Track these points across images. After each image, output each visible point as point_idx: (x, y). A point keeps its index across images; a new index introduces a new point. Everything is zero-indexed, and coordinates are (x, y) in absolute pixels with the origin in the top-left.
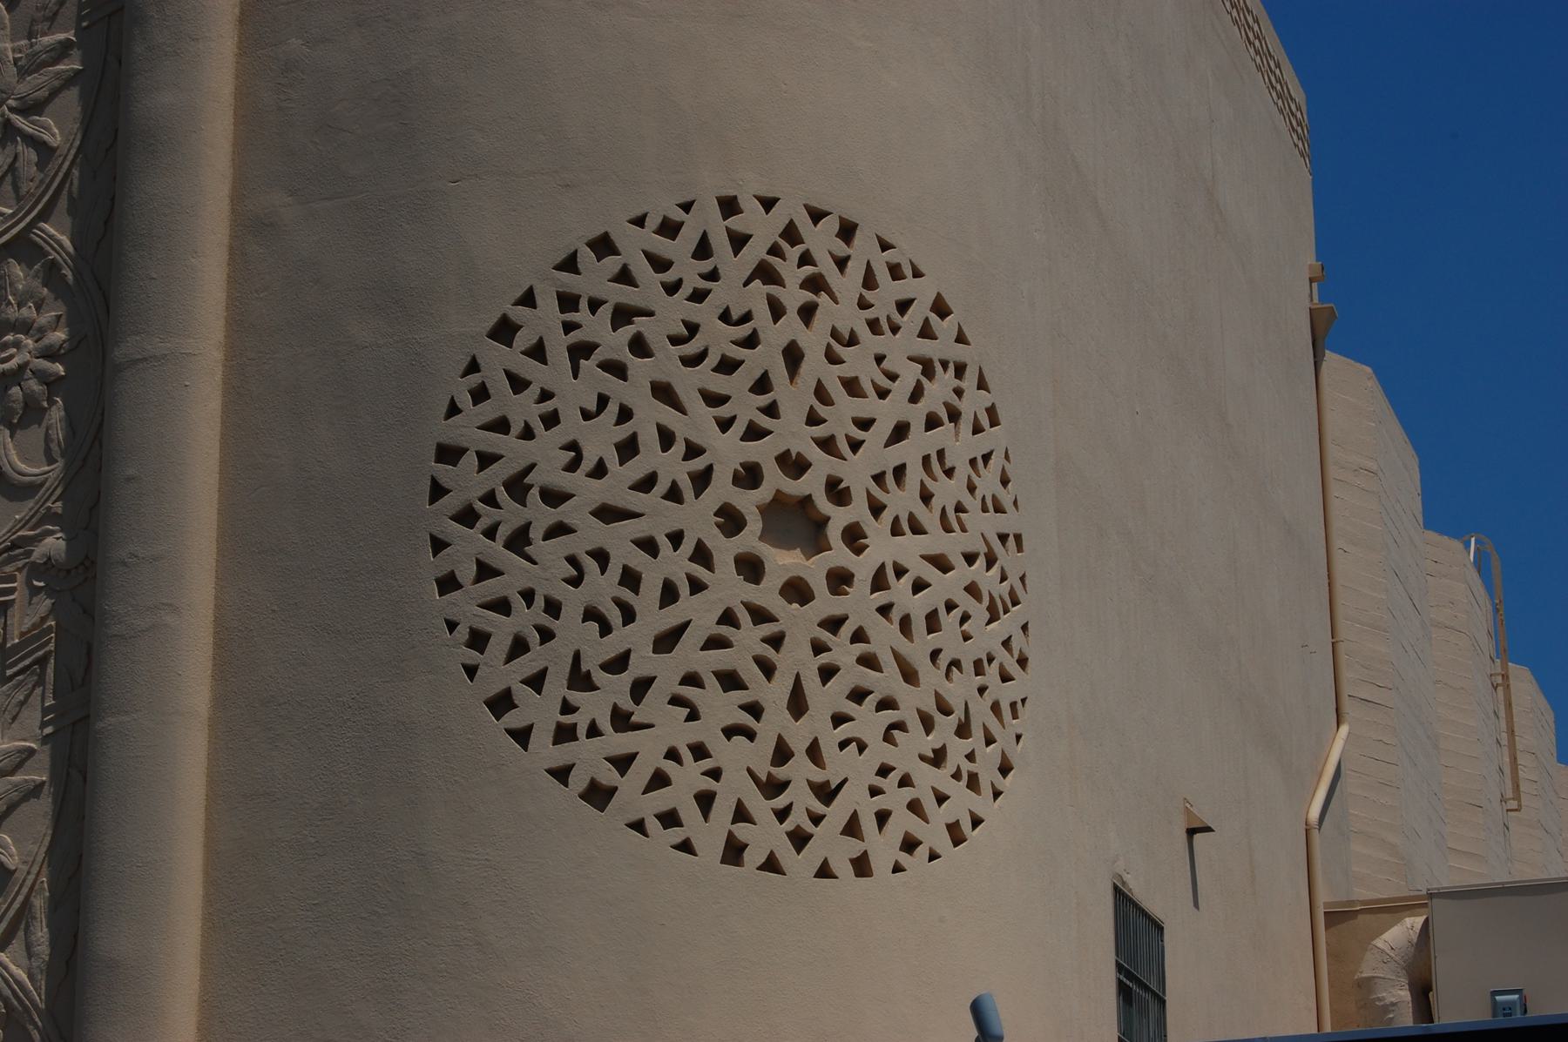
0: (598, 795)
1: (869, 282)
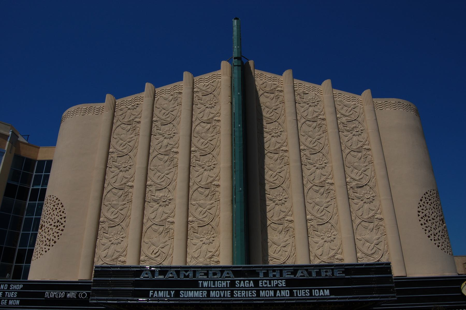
1: (60, 212)
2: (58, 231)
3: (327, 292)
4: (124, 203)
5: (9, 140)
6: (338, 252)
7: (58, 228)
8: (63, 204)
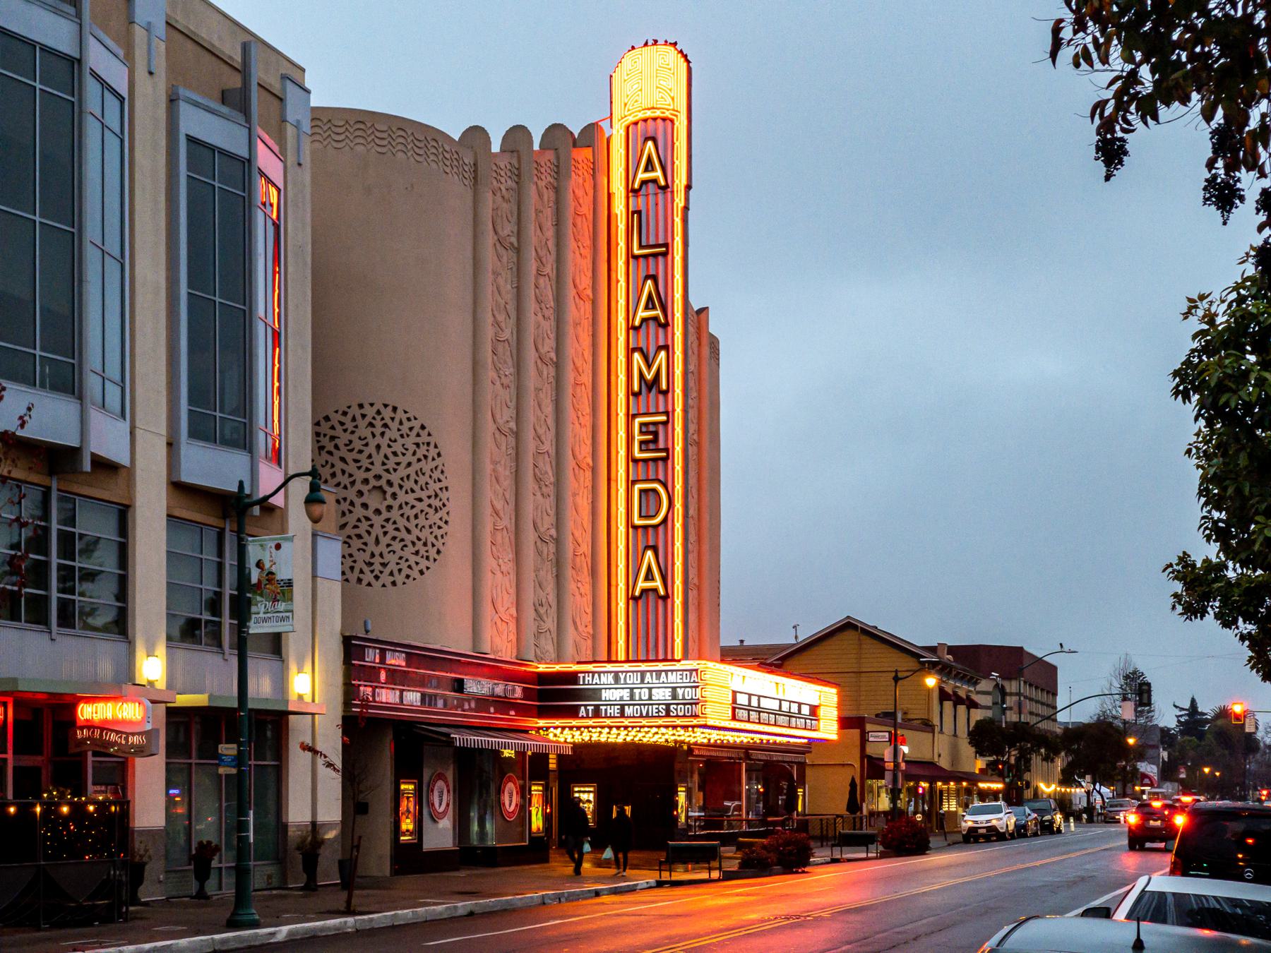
0: (438, 552)
2: (397, 421)
3: (518, 693)
7: (430, 459)
8: (391, 404)
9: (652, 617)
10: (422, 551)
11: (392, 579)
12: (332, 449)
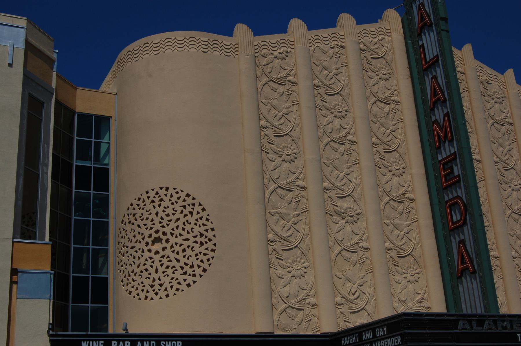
0: (205, 270)
4: (297, 213)
5: (55, 69)
6: (311, 294)
8: (204, 205)
9: (245, 40)
10: (189, 209)
11: (210, 231)
12: (196, 239)
